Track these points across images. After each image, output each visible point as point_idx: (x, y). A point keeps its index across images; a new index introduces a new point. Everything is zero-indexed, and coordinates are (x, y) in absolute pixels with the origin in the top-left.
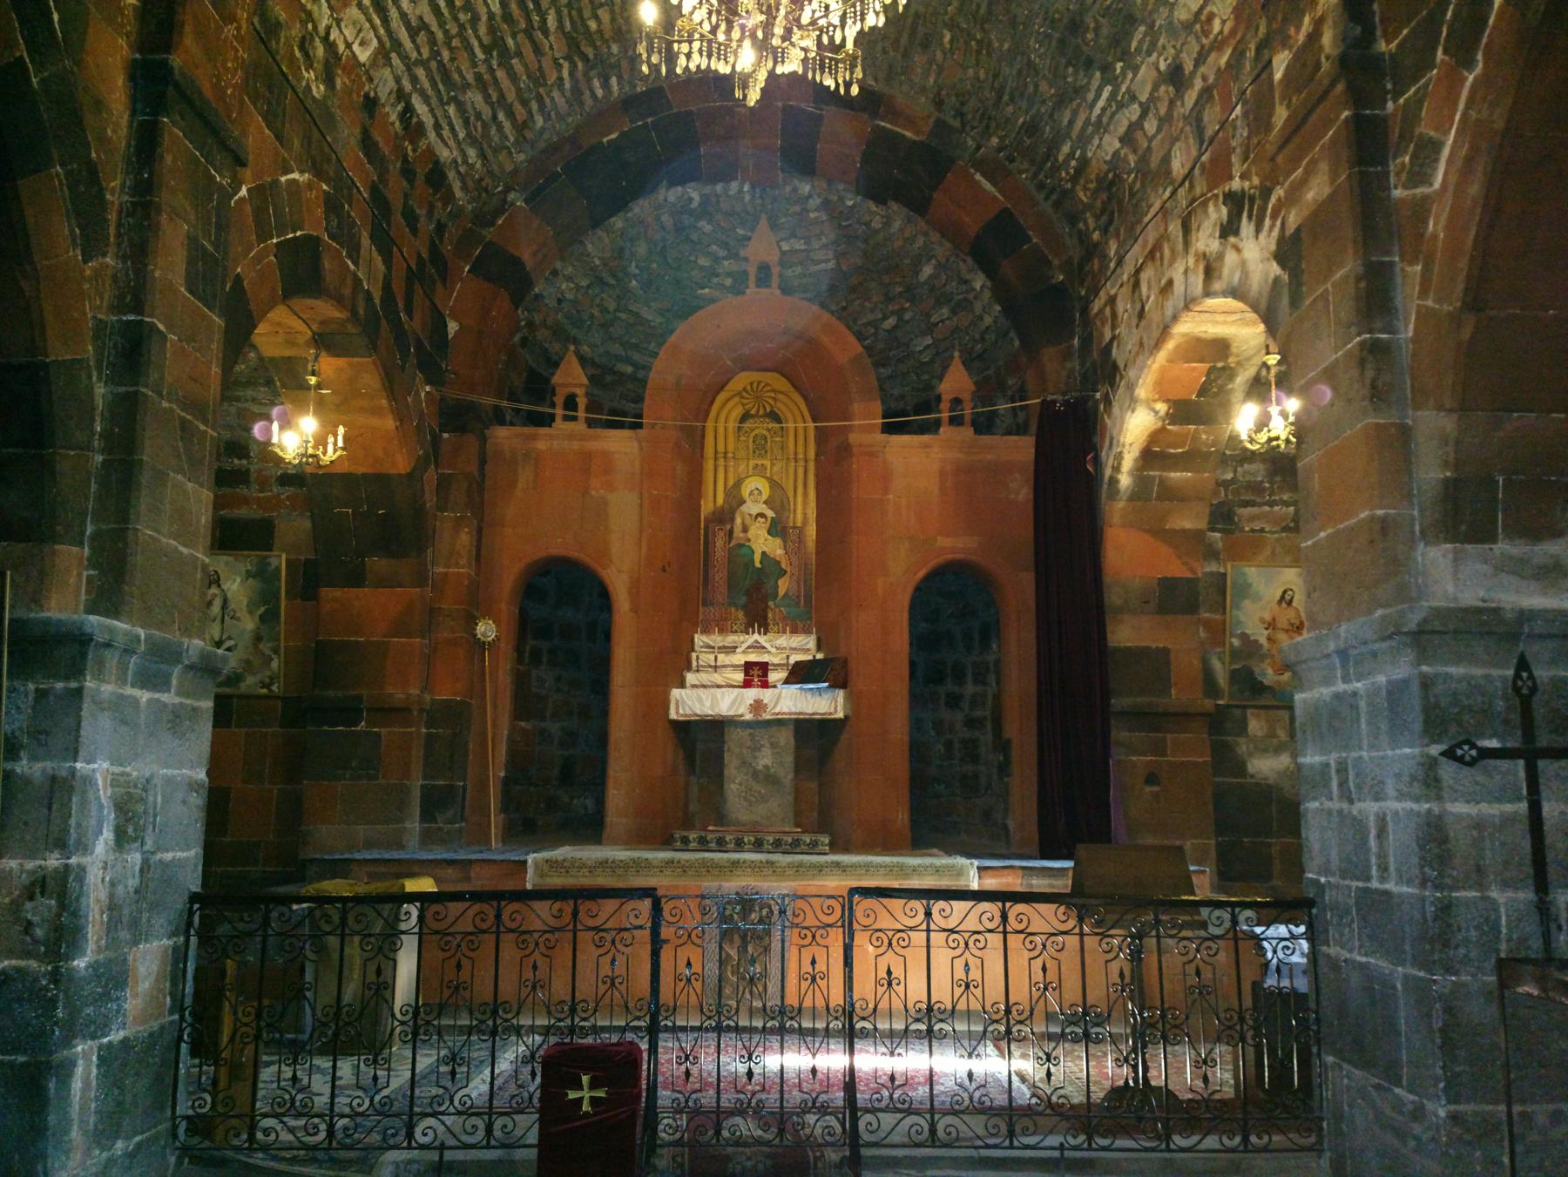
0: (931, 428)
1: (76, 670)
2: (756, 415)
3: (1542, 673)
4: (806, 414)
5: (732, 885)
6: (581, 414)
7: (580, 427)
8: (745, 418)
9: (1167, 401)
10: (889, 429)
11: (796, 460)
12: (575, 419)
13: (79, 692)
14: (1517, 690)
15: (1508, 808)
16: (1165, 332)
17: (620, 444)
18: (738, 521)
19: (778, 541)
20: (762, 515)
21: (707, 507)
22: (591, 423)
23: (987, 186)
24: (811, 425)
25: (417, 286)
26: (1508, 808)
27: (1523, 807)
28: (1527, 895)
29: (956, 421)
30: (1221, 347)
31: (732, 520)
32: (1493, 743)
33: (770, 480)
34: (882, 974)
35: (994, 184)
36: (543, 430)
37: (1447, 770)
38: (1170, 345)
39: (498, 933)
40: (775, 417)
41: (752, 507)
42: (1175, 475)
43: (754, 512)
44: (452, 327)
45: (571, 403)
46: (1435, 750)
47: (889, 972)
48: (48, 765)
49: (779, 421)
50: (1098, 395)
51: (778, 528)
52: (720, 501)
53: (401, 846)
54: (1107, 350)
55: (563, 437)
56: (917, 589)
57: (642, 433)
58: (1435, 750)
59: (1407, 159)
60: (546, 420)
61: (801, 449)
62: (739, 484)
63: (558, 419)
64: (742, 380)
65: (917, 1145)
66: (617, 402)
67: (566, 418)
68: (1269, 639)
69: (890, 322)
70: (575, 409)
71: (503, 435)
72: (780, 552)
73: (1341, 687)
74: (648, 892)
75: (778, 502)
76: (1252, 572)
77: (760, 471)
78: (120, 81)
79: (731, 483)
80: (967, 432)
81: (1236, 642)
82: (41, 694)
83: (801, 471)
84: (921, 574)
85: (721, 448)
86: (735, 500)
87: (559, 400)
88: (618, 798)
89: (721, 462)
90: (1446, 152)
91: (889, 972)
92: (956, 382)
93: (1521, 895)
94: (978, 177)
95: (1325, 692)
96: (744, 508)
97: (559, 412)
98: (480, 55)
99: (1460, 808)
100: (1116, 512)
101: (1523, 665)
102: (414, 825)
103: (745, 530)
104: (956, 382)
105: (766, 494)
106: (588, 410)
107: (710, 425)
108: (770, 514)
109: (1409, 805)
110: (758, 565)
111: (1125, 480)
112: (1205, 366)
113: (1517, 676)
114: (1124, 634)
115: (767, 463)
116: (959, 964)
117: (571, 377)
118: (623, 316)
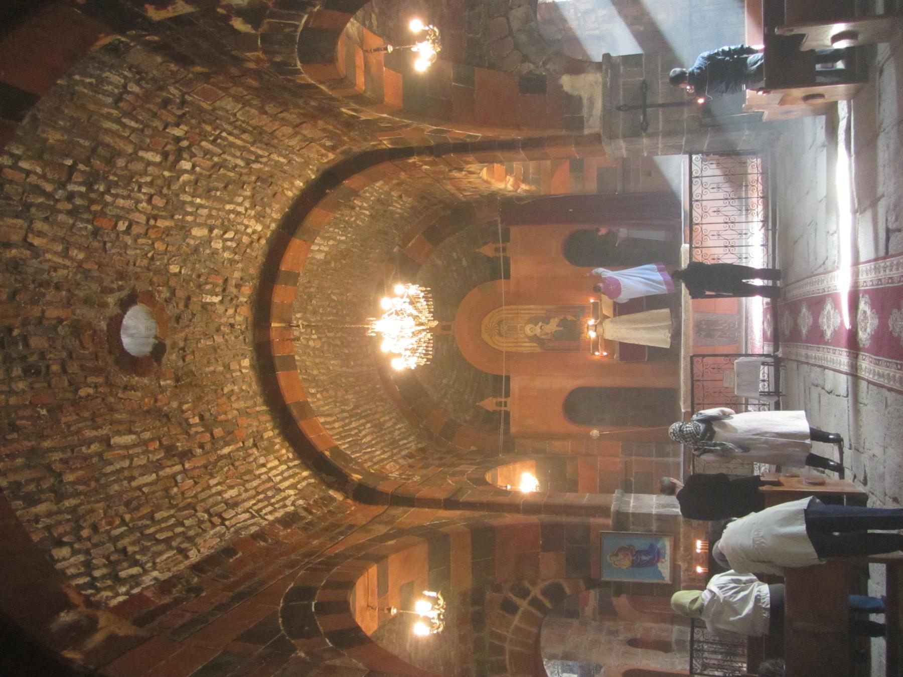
0: (507, 261)
1: (626, 515)
3: (622, 103)
5: (691, 333)
6: (503, 400)
7: (509, 400)
8: (500, 335)
10: (507, 276)
12: (505, 403)
13: (633, 514)
15: (660, 113)
17: (515, 385)
21: (538, 350)
22: (507, 395)
23: (413, 241)
26: (660, 113)
27: (660, 110)
28: (686, 109)
29: (504, 250)
31: (543, 339)
32: (642, 117)
33: (526, 324)
40: (500, 322)
41: (538, 331)
42: (531, 171)
43: (539, 330)
44: (473, 448)
46: (644, 134)
48: (654, 521)
51: (546, 320)
53: (679, 463)
54: (482, 196)
56: (631, 300)
57: (511, 376)
60: (507, 414)
62: (528, 337)
64: (485, 337)
66: (499, 385)
67: (506, 406)
70: (501, 402)
71: (513, 429)
74: (692, 358)
75: (534, 321)
78: (450, 512)
79: (527, 340)
80: (508, 245)
82: (634, 524)
86: (534, 339)
87: (499, 409)
88: (661, 383)
92: (487, 251)
94: (410, 245)
97: (503, 409)
100: (543, 191)
101: (619, 108)
102: (671, 460)
103: (547, 334)
104: (487, 251)
108: (540, 324)
111: (533, 188)
114: (592, 187)
117: (489, 404)
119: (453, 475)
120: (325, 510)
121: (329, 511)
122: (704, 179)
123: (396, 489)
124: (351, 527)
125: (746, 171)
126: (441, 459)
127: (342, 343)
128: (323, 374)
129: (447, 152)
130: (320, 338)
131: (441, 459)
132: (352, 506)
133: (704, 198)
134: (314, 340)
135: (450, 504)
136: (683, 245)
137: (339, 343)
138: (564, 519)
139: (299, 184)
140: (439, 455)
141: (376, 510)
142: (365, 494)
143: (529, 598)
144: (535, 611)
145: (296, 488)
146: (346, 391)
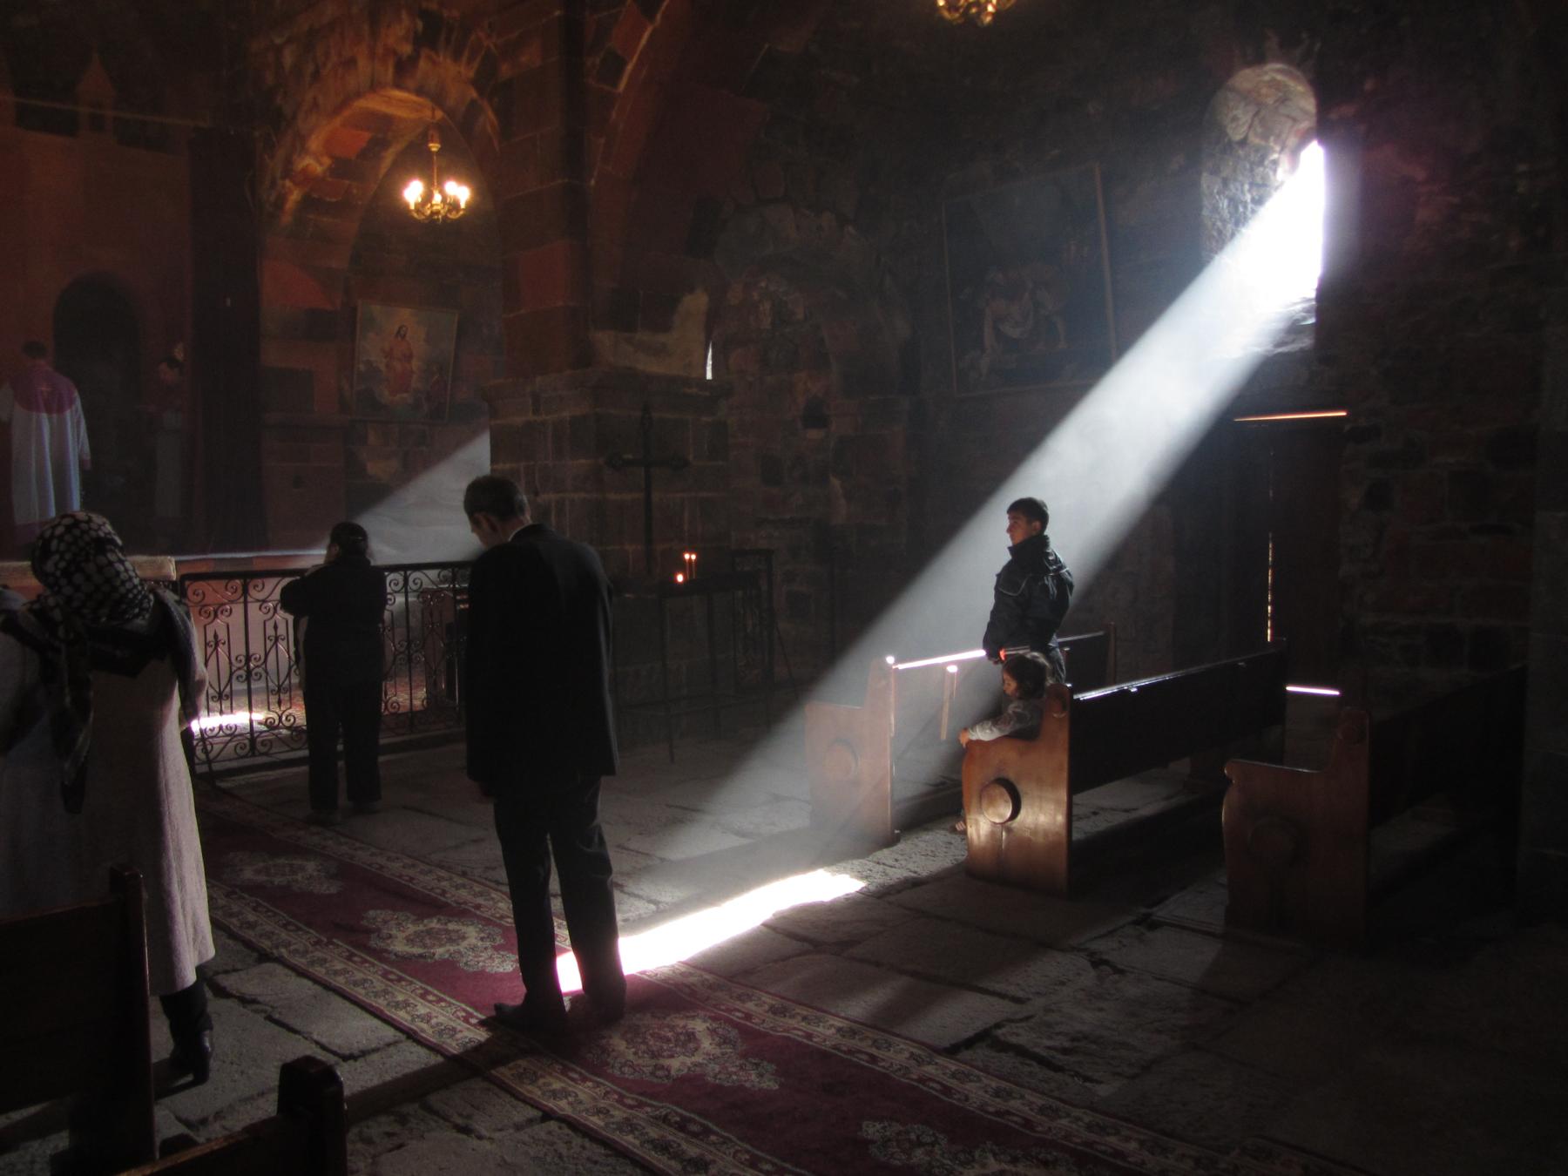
9: (332, 157)
16: (345, 103)
30: (387, 121)
32: (630, 456)
34: (210, 637)
38: (347, 113)
39: (246, 603)
47: (216, 636)
50: (257, 134)
59: (598, 61)
65: (245, 756)
68: (387, 366)
73: (531, 417)
76: (376, 309)
81: (362, 367)
90: (629, 67)
91: (216, 636)
95: (519, 420)
99: (612, 496)
109: (583, 495)
112: (367, 135)
116: (270, 625)
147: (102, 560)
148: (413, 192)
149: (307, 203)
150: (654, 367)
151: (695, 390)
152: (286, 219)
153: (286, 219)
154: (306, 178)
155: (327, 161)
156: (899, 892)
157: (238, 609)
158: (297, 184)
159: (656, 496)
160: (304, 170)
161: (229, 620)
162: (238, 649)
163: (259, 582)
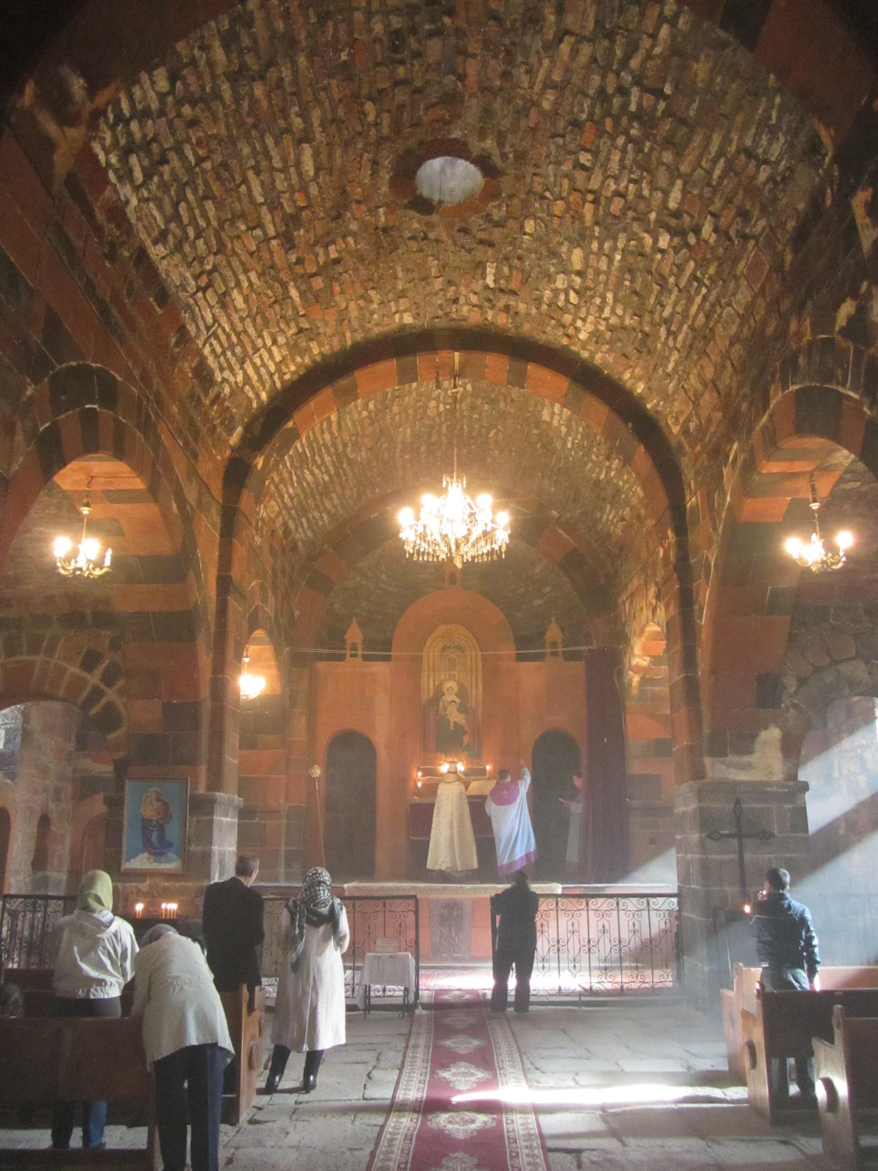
1: (211, 812)
2: (449, 647)
4: (477, 648)
8: (444, 648)
10: (520, 658)
11: (471, 671)
12: (356, 656)
14: (735, 812)
15: (731, 856)
17: (379, 668)
18: (441, 704)
19: (463, 716)
20: (454, 702)
21: (425, 698)
22: (366, 658)
24: (480, 653)
25: (285, 603)
27: (735, 856)
29: (554, 654)
31: (438, 704)
32: (726, 832)
35: (568, 534)
36: (340, 663)
37: (709, 843)
38: (646, 634)
40: (460, 648)
41: (449, 697)
43: (449, 699)
44: (297, 613)
45: (354, 647)
46: (704, 835)
49: (463, 652)
51: (463, 709)
52: (431, 694)
53: (277, 880)
54: (623, 625)
55: (350, 666)
58: (704, 835)
61: (474, 665)
63: (348, 656)
64: (441, 629)
69: (522, 590)
70: (356, 649)
72: (463, 721)
74: (415, 897)
75: (462, 693)
77: (452, 678)
79: (437, 684)
82: (198, 822)
83: (474, 679)
84: (538, 735)
85: (431, 666)
86: (439, 693)
87: (348, 646)
89: (432, 673)
91: (604, 927)
92: (553, 632)
93: (736, 889)
96: (444, 698)
97: (348, 652)
98: (318, 497)
101: (738, 802)
103: (445, 710)
104: (553, 632)
105: (456, 689)
106: (364, 649)
107: (425, 654)
108: (458, 701)
110: (452, 728)
113: (735, 807)
114: (636, 767)
115: (456, 673)
116: (631, 923)
117: (354, 634)
118: (378, 591)
119: (262, 587)
120: (217, 422)
121: (215, 427)
122: (645, 913)
123: (243, 513)
124: (195, 455)
125: (656, 968)
126: (283, 572)
127: (433, 444)
128: (393, 419)
129: (681, 580)
130: (439, 414)
131: (283, 572)
132: (222, 457)
133: (652, 913)
134: (438, 407)
135: (225, 583)
136: (560, 886)
137: (433, 439)
138: (205, 731)
139: (640, 388)
140: (288, 569)
141: (217, 487)
142: (237, 473)
143: (102, 686)
144: (85, 693)
145: (245, 384)
146: (370, 449)
147: (317, 888)
148: (164, 906)
149: (643, 680)
150: (743, 776)
151: (775, 788)
152: (635, 691)
153: (635, 691)
154: (638, 669)
155: (648, 659)
156: (637, 1073)
157: (584, 913)
158: (635, 673)
159: (747, 857)
160: (636, 665)
161: (579, 919)
162: (584, 934)
163: (593, 900)
